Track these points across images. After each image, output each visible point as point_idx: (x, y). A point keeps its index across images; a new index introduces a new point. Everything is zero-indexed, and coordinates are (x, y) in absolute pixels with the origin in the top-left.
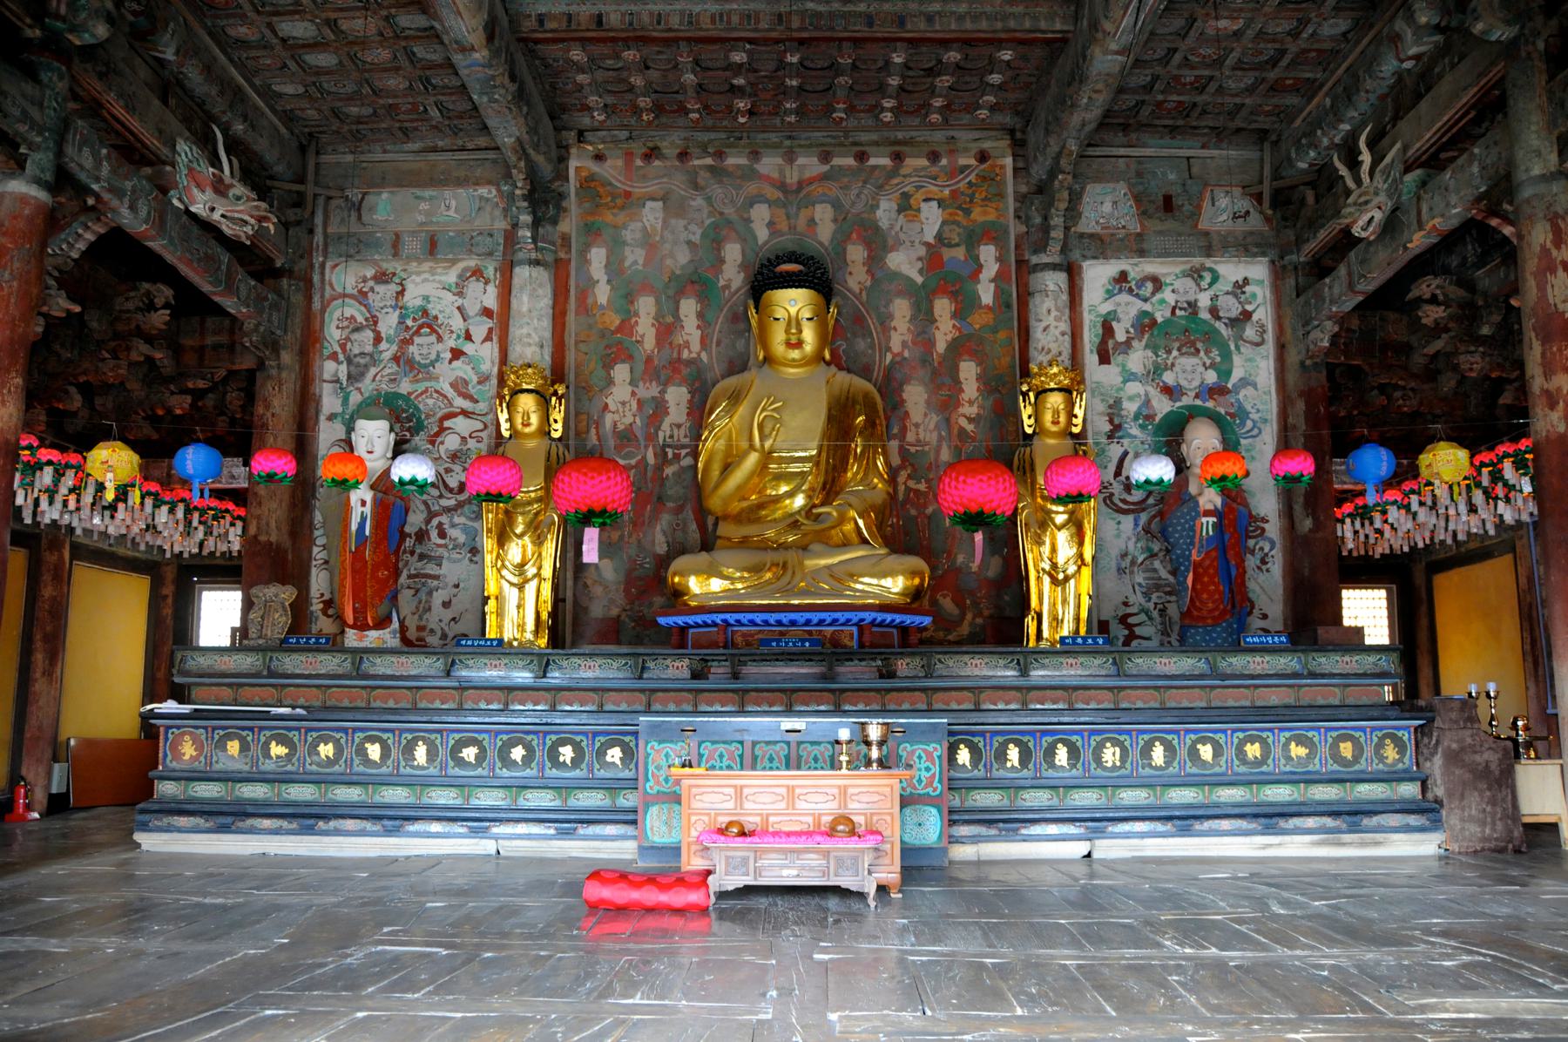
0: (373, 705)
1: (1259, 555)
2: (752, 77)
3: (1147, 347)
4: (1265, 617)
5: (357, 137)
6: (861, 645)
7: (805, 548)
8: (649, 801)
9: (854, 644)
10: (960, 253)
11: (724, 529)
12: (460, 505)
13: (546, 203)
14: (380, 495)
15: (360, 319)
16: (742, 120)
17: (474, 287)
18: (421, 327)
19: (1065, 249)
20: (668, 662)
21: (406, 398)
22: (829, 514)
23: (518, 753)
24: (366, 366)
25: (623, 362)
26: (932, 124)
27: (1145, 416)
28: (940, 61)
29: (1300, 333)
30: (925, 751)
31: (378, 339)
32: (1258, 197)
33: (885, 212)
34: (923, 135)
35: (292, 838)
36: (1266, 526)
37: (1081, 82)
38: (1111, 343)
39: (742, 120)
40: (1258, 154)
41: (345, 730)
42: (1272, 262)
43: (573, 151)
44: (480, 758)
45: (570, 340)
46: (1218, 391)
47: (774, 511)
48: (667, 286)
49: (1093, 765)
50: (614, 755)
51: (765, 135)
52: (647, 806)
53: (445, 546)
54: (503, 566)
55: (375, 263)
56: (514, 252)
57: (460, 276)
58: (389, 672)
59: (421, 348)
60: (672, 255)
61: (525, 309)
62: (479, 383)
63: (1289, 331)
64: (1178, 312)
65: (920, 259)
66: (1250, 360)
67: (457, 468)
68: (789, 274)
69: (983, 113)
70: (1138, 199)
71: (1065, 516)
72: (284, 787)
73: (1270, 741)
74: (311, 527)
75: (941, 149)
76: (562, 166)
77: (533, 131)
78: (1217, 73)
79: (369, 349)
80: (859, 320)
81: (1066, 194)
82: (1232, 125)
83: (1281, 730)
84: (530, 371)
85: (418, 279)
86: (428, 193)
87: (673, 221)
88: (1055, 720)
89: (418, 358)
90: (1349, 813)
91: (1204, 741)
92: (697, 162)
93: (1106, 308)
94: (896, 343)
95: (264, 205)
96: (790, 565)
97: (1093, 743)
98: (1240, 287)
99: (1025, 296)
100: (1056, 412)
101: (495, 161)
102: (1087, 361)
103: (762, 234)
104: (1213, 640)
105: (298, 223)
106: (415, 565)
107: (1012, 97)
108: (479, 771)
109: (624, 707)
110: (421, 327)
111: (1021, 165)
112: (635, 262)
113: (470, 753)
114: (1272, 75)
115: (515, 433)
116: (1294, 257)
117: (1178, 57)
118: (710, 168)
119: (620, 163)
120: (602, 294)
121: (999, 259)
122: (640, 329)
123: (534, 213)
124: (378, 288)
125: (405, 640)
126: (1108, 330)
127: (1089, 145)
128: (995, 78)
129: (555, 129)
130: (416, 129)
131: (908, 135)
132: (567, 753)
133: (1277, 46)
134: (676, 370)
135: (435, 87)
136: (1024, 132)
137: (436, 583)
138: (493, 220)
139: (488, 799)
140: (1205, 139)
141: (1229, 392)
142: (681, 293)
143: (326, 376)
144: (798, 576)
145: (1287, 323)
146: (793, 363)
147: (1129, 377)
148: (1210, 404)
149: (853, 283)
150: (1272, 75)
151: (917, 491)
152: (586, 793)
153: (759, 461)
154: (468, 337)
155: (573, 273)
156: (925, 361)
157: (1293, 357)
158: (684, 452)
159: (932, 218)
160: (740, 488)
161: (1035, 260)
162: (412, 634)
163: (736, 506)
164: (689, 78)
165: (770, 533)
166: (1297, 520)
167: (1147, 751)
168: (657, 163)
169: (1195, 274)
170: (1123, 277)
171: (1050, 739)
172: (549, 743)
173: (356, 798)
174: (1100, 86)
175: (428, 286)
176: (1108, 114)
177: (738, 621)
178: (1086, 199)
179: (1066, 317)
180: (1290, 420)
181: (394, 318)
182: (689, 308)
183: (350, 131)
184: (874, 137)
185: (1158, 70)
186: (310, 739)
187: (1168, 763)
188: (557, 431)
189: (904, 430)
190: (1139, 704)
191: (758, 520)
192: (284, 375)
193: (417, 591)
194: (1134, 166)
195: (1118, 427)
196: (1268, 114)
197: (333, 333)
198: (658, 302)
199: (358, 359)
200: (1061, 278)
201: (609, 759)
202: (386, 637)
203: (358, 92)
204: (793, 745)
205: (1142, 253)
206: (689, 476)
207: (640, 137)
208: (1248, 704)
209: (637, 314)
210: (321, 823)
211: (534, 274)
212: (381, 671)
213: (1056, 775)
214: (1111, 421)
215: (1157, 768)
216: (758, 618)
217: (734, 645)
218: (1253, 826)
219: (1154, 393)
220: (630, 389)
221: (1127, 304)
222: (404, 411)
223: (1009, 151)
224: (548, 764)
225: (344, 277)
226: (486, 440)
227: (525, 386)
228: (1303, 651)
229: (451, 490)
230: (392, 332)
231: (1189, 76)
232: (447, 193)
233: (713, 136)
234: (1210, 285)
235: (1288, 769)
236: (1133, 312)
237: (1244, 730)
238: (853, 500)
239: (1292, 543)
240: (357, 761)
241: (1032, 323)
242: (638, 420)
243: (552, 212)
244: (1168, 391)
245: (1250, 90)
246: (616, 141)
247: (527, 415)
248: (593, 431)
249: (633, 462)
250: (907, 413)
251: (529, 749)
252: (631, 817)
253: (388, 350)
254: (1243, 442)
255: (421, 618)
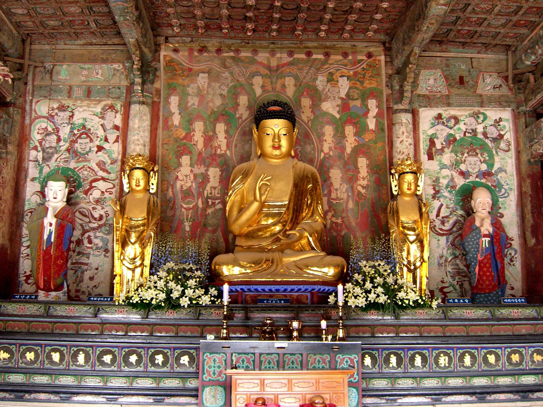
0: (55, 332)
1: (509, 257)
2: (256, 13)
3: (452, 152)
4: (513, 288)
5: (52, 36)
6: (312, 302)
7: (282, 251)
8: (205, 385)
9: (309, 301)
10: (358, 103)
11: (239, 242)
12: (100, 227)
13: (148, 72)
14: (60, 221)
15: (50, 129)
16: (249, 34)
17: (110, 114)
18: (82, 134)
19: (411, 103)
20: (212, 310)
21: (73, 170)
22: (295, 234)
23: (133, 358)
24: (52, 154)
25: (187, 155)
26: (344, 38)
27: (451, 186)
28: (351, 7)
29: (528, 146)
30: (349, 358)
31: (59, 140)
32: (506, 78)
33: (321, 82)
34: (340, 44)
35: (12, 402)
36: (512, 242)
37: (424, 19)
38: (434, 150)
39: (249, 34)
40: (505, 57)
41: (40, 345)
42: (513, 110)
43: (163, 47)
44: (113, 361)
45: (159, 143)
46: (487, 174)
47: (265, 233)
48: (209, 117)
49: (434, 366)
50: (185, 360)
51: (261, 42)
52: (204, 387)
53: (91, 248)
54: (124, 258)
55: (59, 101)
56: (131, 97)
57: (103, 109)
58: (64, 314)
59: (81, 145)
60: (212, 101)
61: (136, 126)
62: (111, 164)
63: (522, 145)
64: (467, 134)
65: (338, 106)
66: (503, 159)
67: (99, 207)
68: (275, 112)
69: (370, 34)
70: (446, 78)
71: (415, 237)
72: (7, 375)
73: (524, 353)
74: (21, 237)
75: (349, 51)
76: (157, 54)
77: (144, 36)
78: (488, 17)
79: (54, 145)
80: (307, 136)
81: (412, 75)
82: (494, 42)
83: (530, 347)
84: (140, 158)
85: (81, 110)
86: (87, 66)
87: (213, 84)
88: (415, 342)
89: (79, 150)
90: (522, 392)
91: (490, 353)
92: (225, 54)
93: (431, 132)
94: (326, 149)
95: (7, 69)
96: (275, 261)
97: (434, 354)
98: (498, 122)
99: (391, 125)
100: (409, 184)
101: (122, 51)
102: (422, 158)
103: (258, 91)
104: (489, 300)
105: (20, 79)
106: (75, 258)
107: (387, 26)
108: (113, 368)
109: (189, 334)
110: (82, 134)
111: (388, 60)
112: (194, 104)
113: (107, 358)
114: (515, 19)
115: (131, 190)
116: (524, 108)
117: (470, 8)
118: (233, 58)
119: (186, 53)
120: (176, 120)
121: (378, 106)
122: (196, 138)
123: (142, 78)
124: (59, 114)
125: (70, 298)
126: (432, 143)
127: (424, 51)
128: (378, 16)
129: (154, 35)
130: (82, 33)
131: (332, 43)
132: (159, 359)
133: (518, 5)
134: (213, 160)
135: (94, 12)
136: (390, 44)
137: (86, 267)
138: (120, 81)
139: (117, 383)
140: (480, 49)
141: (493, 175)
142: (216, 120)
143: (31, 158)
144: (280, 267)
145: (521, 140)
146: (276, 157)
147: (443, 167)
148: (483, 181)
149: (304, 117)
150: (515, 19)
151: (336, 223)
152: (169, 380)
153: (259, 206)
154: (106, 140)
155: (161, 109)
156: (341, 157)
157: (524, 158)
158: (217, 201)
159: (344, 85)
160: (248, 220)
161: (395, 107)
162: (73, 294)
163: (246, 230)
164: (225, 12)
165: (264, 244)
166: (527, 239)
167: (461, 359)
168: (205, 54)
169: (475, 115)
170: (439, 116)
171: (412, 352)
172: (150, 353)
173: (45, 382)
174: (433, 21)
175: (86, 113)
176: (435, 36)
177: (249, 290)
178: (421, 77)
179: (412, 136)
180: (523, 189)
181: (68, 129)
182: (221, 128)
183: (49, 33)
184: (315, 44)
185: (460, 14)
186: (21, 350)
187: (473, 365)
188: (153, 189)
189: (330, 192)
190: (456, 334)
191: (258, 237)
192: (9, 157)
193: (76, 271)
194: (445, 62)
195: (437, 192)
196: (511, 37)
197: (36, 136)
198: (205, 124)
199: (48, 150)
200: (409, 116)
201: (182, 362)
202: (61, 295)
203: (55, 14)
204: (281, 356)
205: (449, 105)
206: (220, 213)
207: (197, 41)
208: (511, 334)
209: (194, 131)
210: (27, 395)
211: (142, 109)
212: (60, 313)
213: (415, 371)
214: (434, 189)
215: (467, 367)
216: (260, 288)
217: (246, 302)
218: (516, 397)
219: (455, 175)
220: (190, 168)
221: (442, 130)
222: (71, 177)
223: (383, 53)
224: (150, 365)
225: (42, 108)
226: (114, 194)
227: (137, 166)
228: (537, 306)
229: (95, 219)
230: (66, 136)
231: (474, 18)
232: (97, 66)
233: (234, 41)
234: (483, 121)
235: (533, 367)
236: (445, 134)
237: (511, 347)
238: (306, 227)
239: (526, 251)
240: (46, 362)
241: (395, 139)
242: (194, 185)
243: (151, 77)
244: (463, 174)
245: (504, 26)
246: (184, 43)
247: (138, 180)
248: (170, 190)
249: (191, 206)
250: (331, 183)
251: (139, 356)
252: (194, 393)
253: (64, 145)
254: (500, 200)
255: (77, 285)
